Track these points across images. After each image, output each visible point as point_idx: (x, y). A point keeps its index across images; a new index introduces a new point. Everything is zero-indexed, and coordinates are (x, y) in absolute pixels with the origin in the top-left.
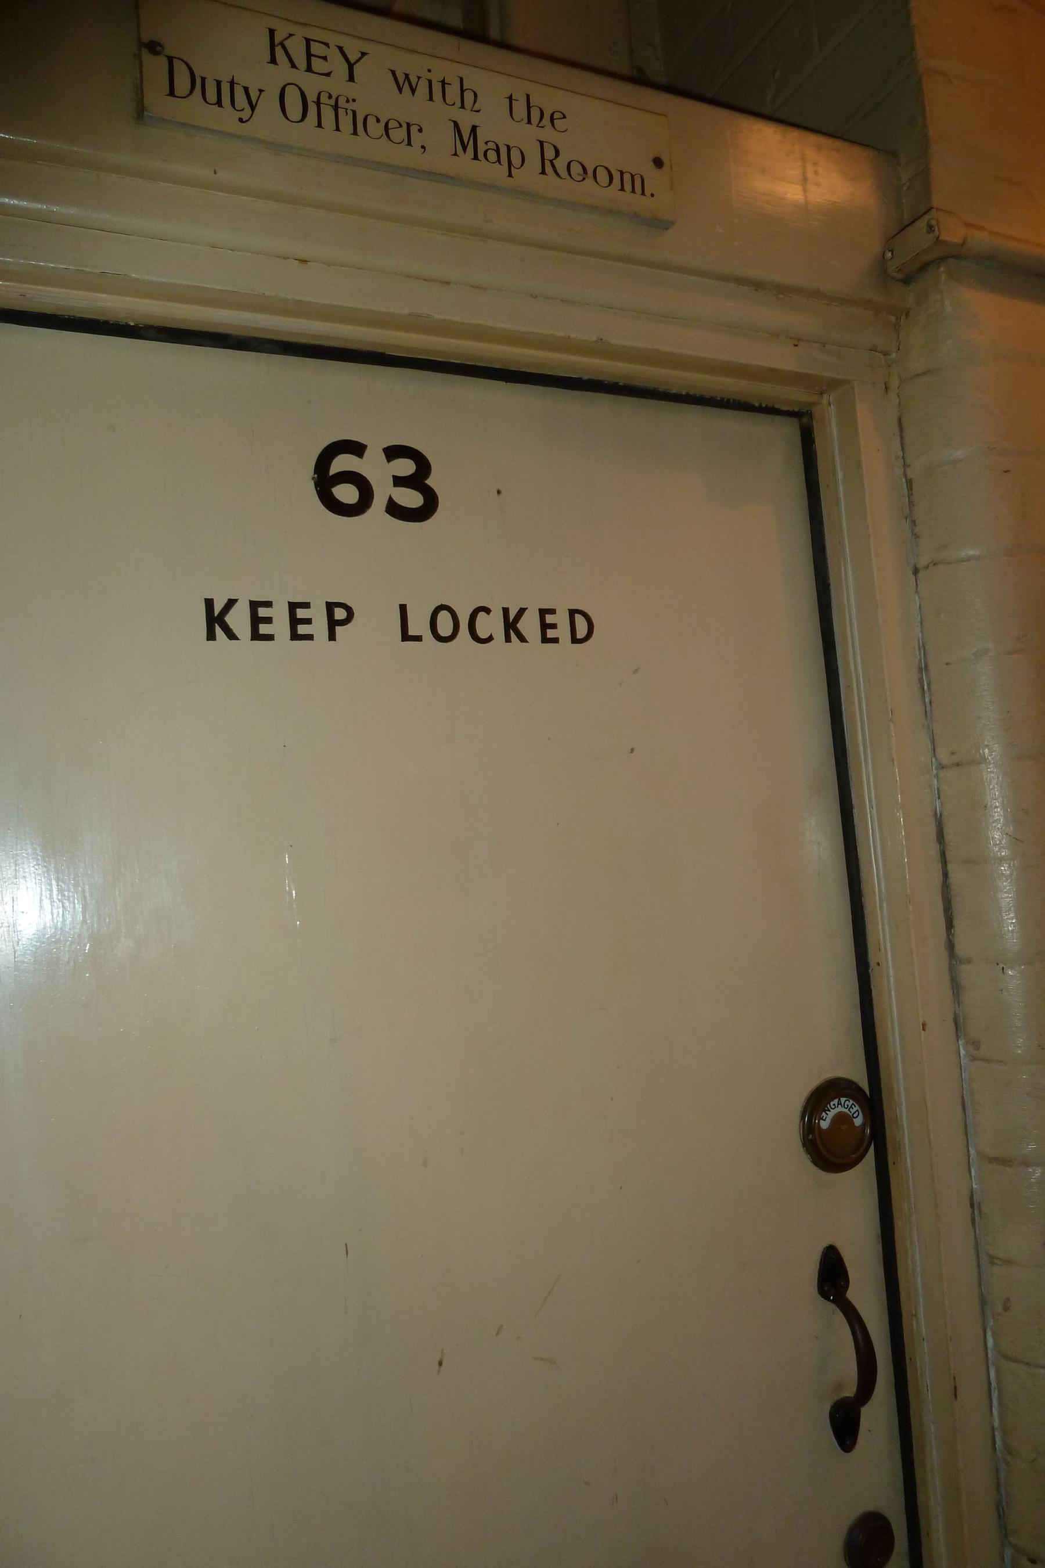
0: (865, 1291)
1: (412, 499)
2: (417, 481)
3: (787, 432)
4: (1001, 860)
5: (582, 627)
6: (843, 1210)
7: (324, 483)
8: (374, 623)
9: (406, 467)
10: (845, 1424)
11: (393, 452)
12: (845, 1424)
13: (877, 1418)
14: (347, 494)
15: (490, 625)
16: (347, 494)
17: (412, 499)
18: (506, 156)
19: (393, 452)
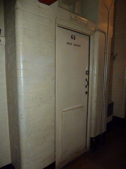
0: (87, 80)
1: (74, 38)
2: (75, 38)
3: (88, 37)
4: (22, 78)
5: (80, 46)
6: (87, 77)
7: (71, 37)
8: (73, 44)
9: (74, 37)
10: (86, 87)
11: (74, 36)
12: (86, 87)
13: (87, 86)
14: (72, 38)
15: (77, 45)
16: (72, 38)
17: (74, 38)
18: (73, 19)
19: (74, 36)
